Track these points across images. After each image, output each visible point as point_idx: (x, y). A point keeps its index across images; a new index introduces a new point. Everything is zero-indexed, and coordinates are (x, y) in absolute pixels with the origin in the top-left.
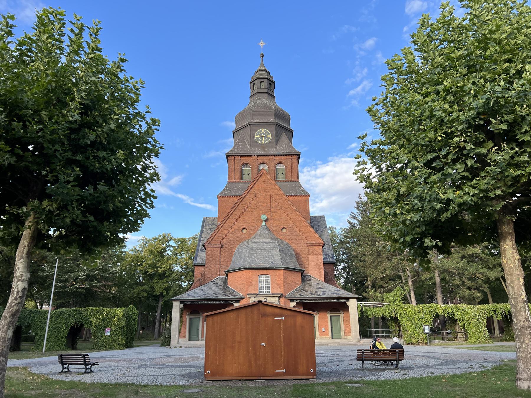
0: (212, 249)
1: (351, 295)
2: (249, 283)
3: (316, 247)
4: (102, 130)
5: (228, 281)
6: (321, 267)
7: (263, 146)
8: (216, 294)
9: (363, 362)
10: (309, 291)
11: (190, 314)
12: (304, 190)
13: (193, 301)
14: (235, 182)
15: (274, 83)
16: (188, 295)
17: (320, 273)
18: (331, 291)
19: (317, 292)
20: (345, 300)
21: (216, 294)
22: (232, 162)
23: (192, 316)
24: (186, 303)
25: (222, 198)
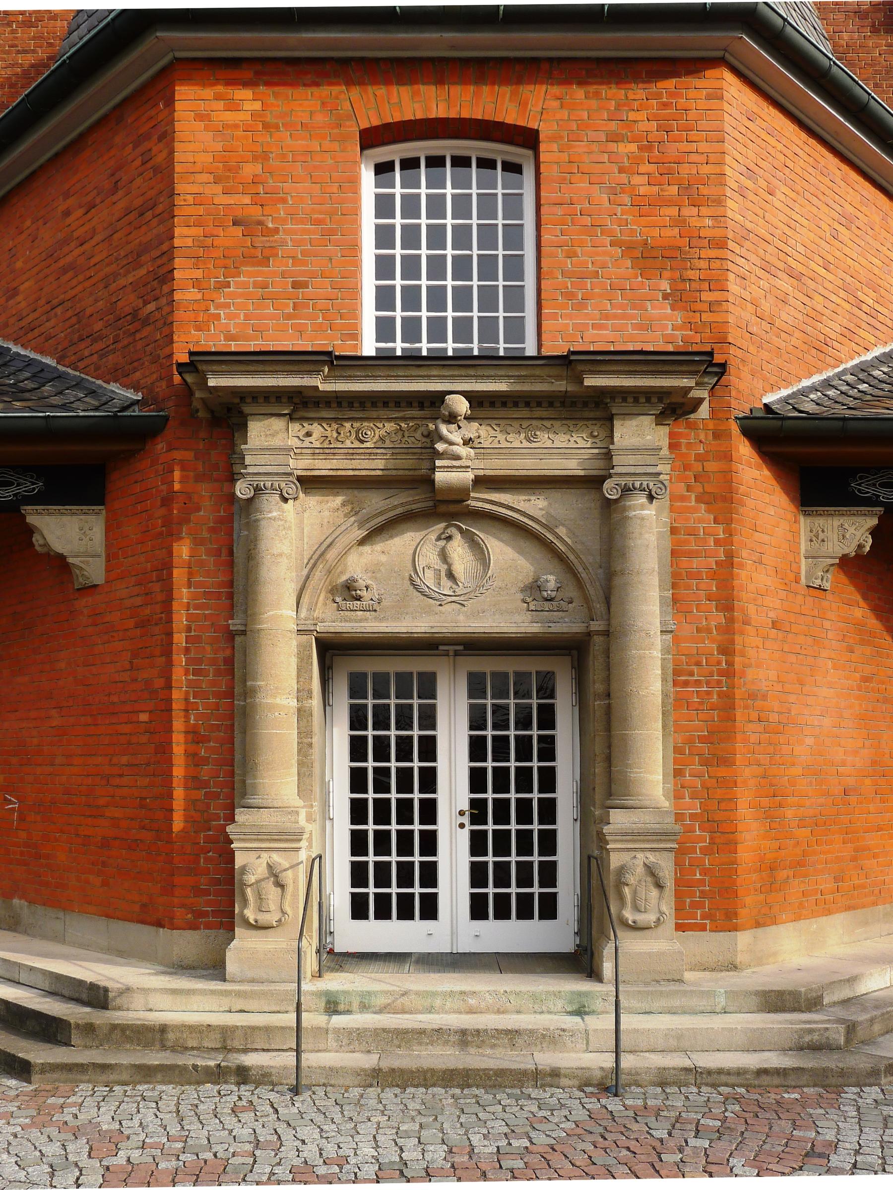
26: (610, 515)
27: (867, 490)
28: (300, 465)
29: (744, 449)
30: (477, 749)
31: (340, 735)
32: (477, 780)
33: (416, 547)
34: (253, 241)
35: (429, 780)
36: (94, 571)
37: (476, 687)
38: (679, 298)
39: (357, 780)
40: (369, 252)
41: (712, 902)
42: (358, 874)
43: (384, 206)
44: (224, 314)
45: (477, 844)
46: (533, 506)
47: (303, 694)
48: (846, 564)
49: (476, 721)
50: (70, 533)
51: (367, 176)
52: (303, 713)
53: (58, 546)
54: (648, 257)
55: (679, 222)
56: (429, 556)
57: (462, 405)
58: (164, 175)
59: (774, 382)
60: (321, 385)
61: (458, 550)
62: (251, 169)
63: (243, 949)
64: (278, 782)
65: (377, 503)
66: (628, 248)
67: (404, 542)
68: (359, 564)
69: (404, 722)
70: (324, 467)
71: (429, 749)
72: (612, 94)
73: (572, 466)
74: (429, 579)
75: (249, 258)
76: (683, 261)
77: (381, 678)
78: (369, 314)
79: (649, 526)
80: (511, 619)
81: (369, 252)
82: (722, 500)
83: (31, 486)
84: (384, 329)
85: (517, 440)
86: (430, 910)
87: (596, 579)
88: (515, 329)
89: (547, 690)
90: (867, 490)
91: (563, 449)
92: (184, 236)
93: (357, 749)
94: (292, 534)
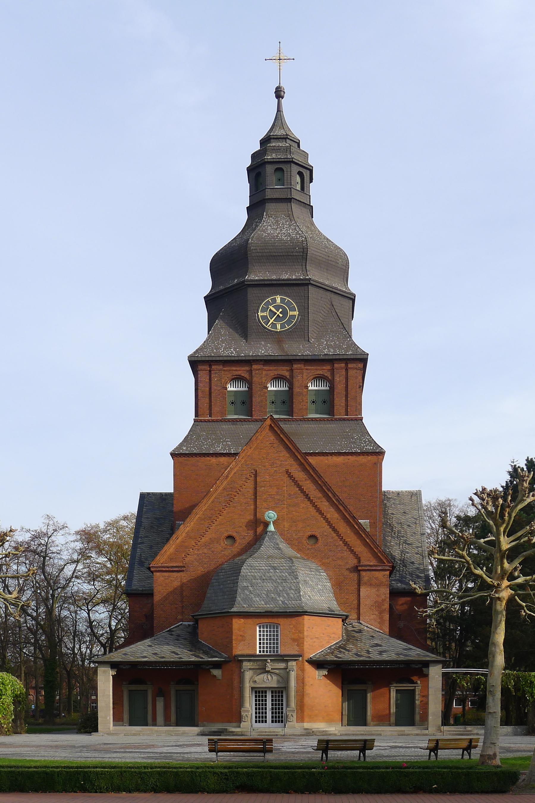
0: (165, 574)
1: (432, 657)
2: (240, 638)
3: (377, 573)
4: (76, 612)
5: (199, 631)
6: (384, 607)
7: (278, 338)
8: (177, 654)
9: (217, 754)
10: (354, 651)
11: (129, 684)
12: (372, 442)
13: (134, 665)
14: (213, 421)
15: (311, 171)
16: (125, 654)
17: (381, 618)
18: (395, 650)
19: (368, 652)
20: (420, 666)
21: (177, 654)
22: (204, 376)
23: (133, 687)
24: (121, 667)
25: (181, 459)
26: (288, 673)
27: (326, 666)
28: (249, 667)
29: (307, 663)
30: (272, 700)
31: (254, 699)
32: (272, 705)
33: (264, 676)
34: (243, 638)
35: (266, 705)
36: (220, 678)
37: (272, 692)
38: (298, 645)
39: (256, 705)
40: (258, 633)
41: (301, 719)
42: (256, 717)
43: (260, 631)
44: (239, 649)
45: (272, 713)
46: (277, 671)
47: (250, 694)
48: (325, 676)
49: (272, 696)
50: (217, 673)
51: (258, 628)
52: (250, 697)
53: (215, 674)
54: (294, 640)
55: (298, 635)
56: (265, 677)
57: (269, 661)
58: (231, 628)
59: (312, 653)
60: (252, 657)
61: (269, 676)
62: (243, 629)
63: (242, 724)
64: (247, 705)
65: (259, 671)
66: (291, 639)
67: (262, 676)
68: (257, 678)
69: (262, 697)
70: (252, 667)
71: (266, 700)
72: (290, 619)
73: (282, 667)
74: (265, 680)
75: (242, 640)
76: (299, 641)
77: (259, 693)
78: (258, 649)
79: (293, 675)
80: (274, 685)
81: (258, 633)
82: (303, 670)
83: (210, 666)
84: (260, 651)
85: (276, 664)
86: (266, 722)
87: (286, 680)
88: (277, 651)
89: (282, 693)
90: (326, 666)
91: (282, 665)
92: (234, 638)
93: (256, 701)
94: (248, 675)
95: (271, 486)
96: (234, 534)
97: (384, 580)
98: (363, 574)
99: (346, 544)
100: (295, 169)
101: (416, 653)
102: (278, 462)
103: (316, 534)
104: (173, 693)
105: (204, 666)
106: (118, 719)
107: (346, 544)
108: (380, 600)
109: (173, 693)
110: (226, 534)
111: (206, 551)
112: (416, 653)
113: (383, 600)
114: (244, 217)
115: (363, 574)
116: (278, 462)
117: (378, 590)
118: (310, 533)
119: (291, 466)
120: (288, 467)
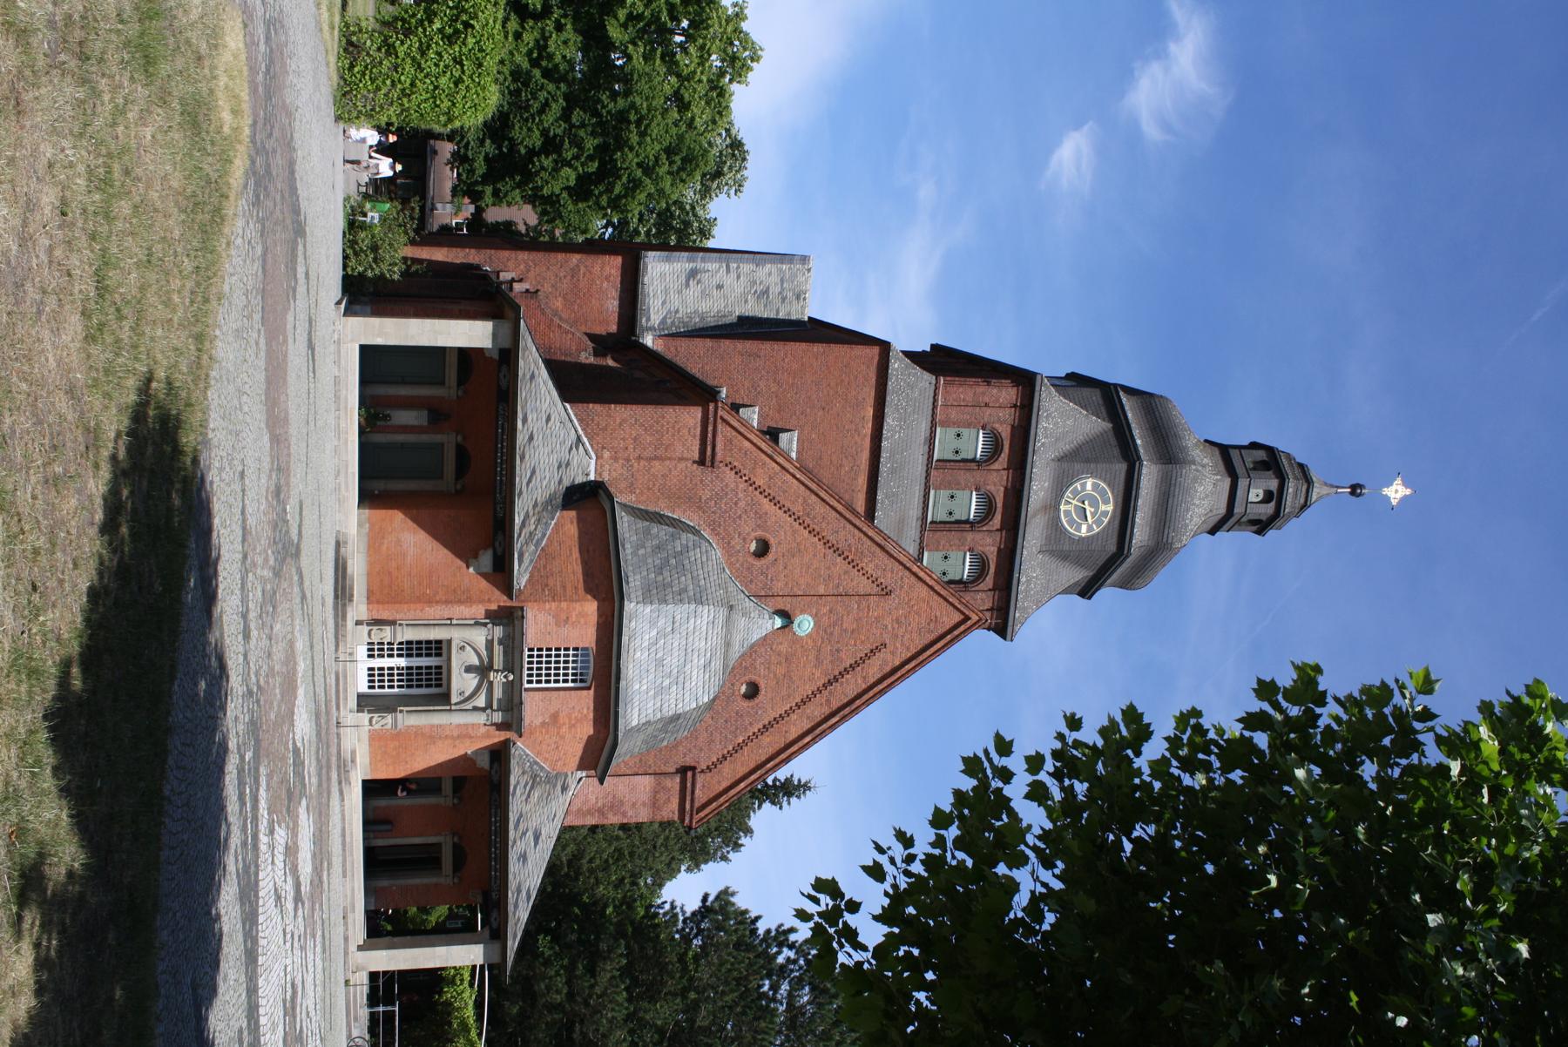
1: (513, 945)
6: (610, 816)
17: (590, 812)
38: (543, 724)
54: (555, 717)
92: (564, 605)
95: (858, 620)
96: (771, 557)
97: (664, 813)
98: (612, 266)
99: (739, 748)
100: (1273, 484)
101: (520, 913)
102: (902, 630)
103: (760, 697)
104: (438, 438)
105: (500, 537)
106: (371, 356)
107: (739, 748)
108: (627, 807)
109: (438, 438)
110: (772, 541)
111: (742, 504)
112: (520, 913)
113: (624, 814)
114: (1246, 443)
115: (612, 266)
116: (902, 630)
117: (644, 804)
118: (762, 686)
119: (893, 653)
120: (890, 647)
